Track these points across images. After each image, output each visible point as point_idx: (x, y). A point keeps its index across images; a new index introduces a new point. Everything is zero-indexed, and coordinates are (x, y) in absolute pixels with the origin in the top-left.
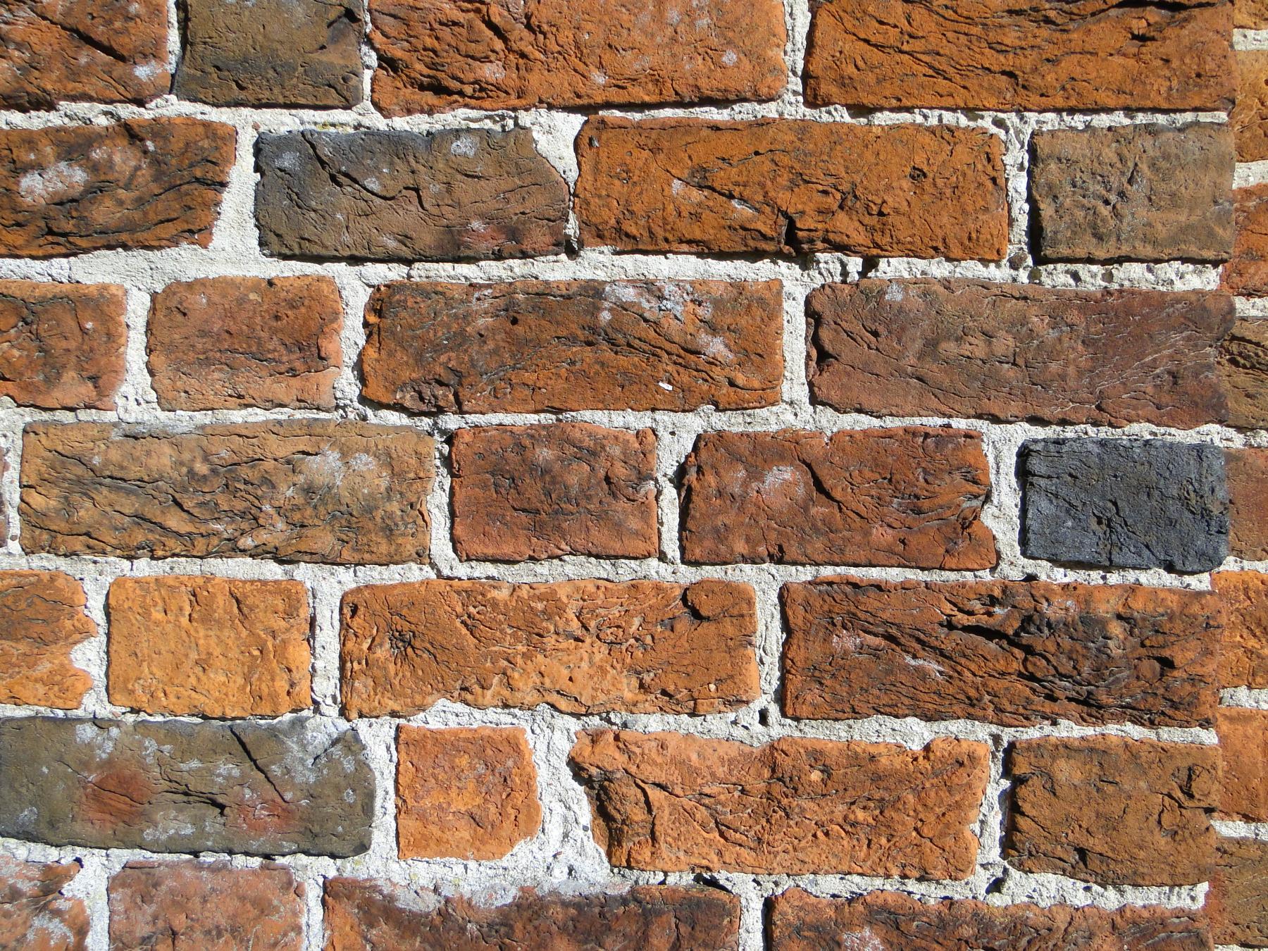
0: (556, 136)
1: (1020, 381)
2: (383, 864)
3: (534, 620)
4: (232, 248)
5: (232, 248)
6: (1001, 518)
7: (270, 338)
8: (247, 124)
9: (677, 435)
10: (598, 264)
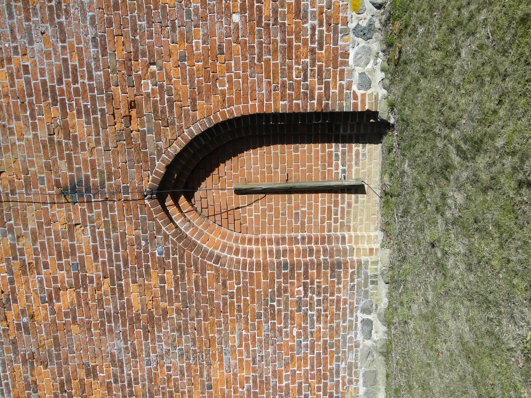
0: (270, 290)
1: (280, 271)
2: (302, 296)
3: (291, 290)
4: (275, 304)
5: (275, 304)
6: (286, 271)
7: (279, 302)
8: (269, 303)
9: (283, 285)
10: (275, 288)
